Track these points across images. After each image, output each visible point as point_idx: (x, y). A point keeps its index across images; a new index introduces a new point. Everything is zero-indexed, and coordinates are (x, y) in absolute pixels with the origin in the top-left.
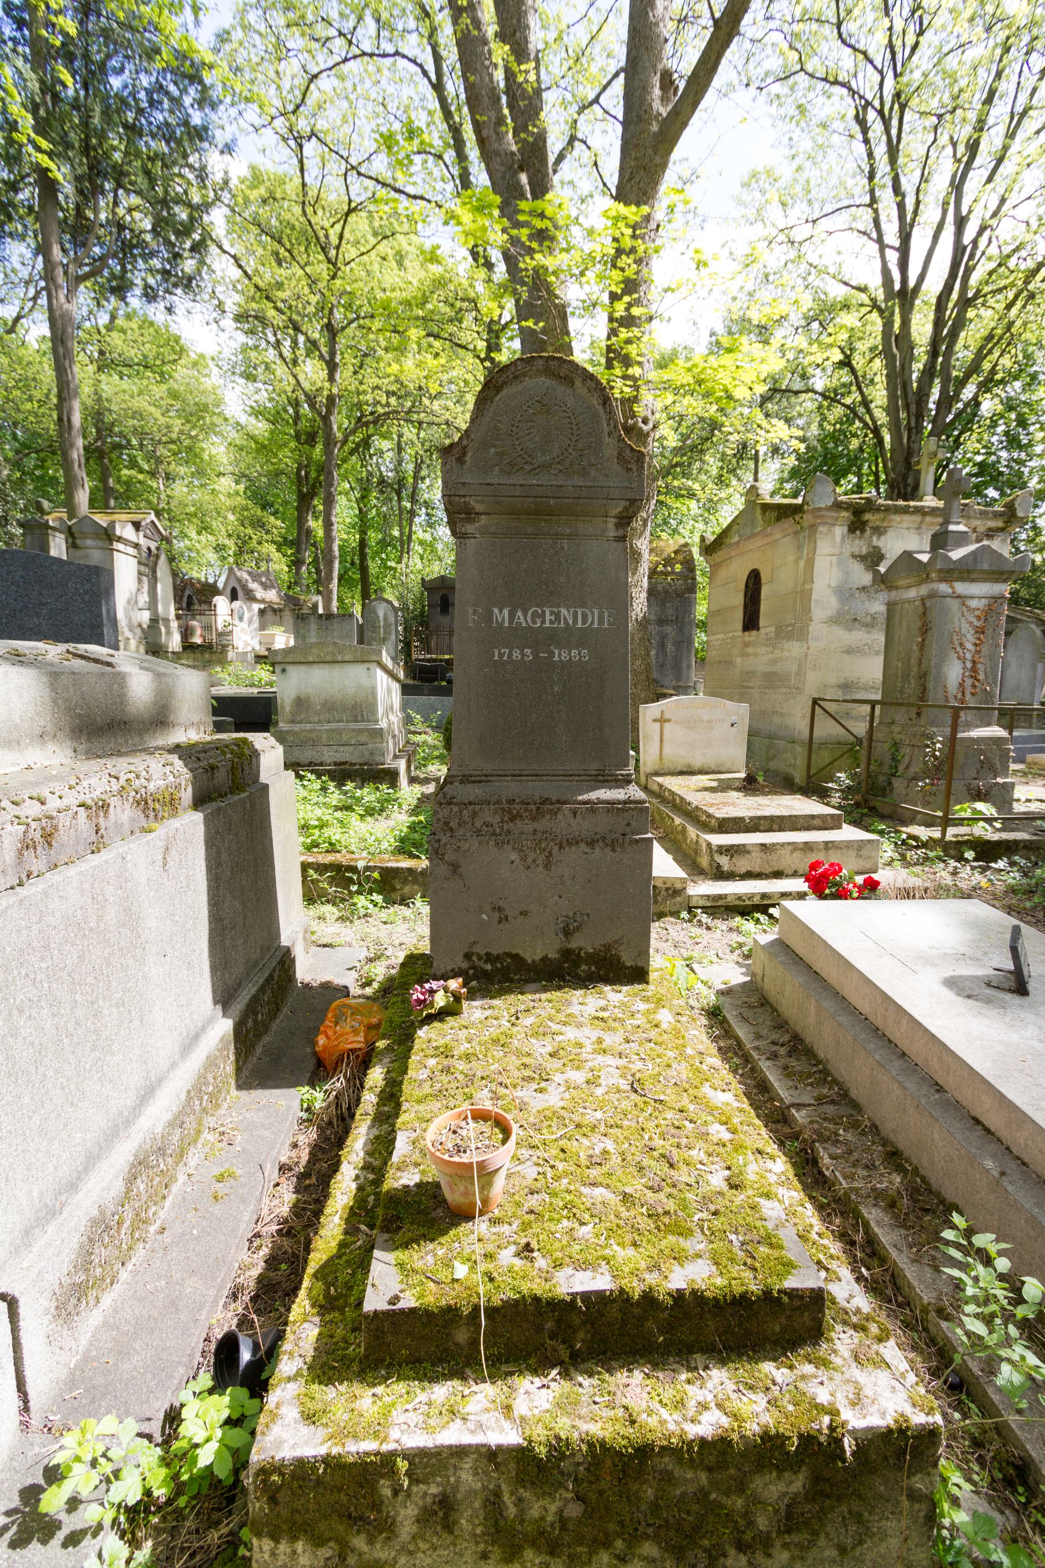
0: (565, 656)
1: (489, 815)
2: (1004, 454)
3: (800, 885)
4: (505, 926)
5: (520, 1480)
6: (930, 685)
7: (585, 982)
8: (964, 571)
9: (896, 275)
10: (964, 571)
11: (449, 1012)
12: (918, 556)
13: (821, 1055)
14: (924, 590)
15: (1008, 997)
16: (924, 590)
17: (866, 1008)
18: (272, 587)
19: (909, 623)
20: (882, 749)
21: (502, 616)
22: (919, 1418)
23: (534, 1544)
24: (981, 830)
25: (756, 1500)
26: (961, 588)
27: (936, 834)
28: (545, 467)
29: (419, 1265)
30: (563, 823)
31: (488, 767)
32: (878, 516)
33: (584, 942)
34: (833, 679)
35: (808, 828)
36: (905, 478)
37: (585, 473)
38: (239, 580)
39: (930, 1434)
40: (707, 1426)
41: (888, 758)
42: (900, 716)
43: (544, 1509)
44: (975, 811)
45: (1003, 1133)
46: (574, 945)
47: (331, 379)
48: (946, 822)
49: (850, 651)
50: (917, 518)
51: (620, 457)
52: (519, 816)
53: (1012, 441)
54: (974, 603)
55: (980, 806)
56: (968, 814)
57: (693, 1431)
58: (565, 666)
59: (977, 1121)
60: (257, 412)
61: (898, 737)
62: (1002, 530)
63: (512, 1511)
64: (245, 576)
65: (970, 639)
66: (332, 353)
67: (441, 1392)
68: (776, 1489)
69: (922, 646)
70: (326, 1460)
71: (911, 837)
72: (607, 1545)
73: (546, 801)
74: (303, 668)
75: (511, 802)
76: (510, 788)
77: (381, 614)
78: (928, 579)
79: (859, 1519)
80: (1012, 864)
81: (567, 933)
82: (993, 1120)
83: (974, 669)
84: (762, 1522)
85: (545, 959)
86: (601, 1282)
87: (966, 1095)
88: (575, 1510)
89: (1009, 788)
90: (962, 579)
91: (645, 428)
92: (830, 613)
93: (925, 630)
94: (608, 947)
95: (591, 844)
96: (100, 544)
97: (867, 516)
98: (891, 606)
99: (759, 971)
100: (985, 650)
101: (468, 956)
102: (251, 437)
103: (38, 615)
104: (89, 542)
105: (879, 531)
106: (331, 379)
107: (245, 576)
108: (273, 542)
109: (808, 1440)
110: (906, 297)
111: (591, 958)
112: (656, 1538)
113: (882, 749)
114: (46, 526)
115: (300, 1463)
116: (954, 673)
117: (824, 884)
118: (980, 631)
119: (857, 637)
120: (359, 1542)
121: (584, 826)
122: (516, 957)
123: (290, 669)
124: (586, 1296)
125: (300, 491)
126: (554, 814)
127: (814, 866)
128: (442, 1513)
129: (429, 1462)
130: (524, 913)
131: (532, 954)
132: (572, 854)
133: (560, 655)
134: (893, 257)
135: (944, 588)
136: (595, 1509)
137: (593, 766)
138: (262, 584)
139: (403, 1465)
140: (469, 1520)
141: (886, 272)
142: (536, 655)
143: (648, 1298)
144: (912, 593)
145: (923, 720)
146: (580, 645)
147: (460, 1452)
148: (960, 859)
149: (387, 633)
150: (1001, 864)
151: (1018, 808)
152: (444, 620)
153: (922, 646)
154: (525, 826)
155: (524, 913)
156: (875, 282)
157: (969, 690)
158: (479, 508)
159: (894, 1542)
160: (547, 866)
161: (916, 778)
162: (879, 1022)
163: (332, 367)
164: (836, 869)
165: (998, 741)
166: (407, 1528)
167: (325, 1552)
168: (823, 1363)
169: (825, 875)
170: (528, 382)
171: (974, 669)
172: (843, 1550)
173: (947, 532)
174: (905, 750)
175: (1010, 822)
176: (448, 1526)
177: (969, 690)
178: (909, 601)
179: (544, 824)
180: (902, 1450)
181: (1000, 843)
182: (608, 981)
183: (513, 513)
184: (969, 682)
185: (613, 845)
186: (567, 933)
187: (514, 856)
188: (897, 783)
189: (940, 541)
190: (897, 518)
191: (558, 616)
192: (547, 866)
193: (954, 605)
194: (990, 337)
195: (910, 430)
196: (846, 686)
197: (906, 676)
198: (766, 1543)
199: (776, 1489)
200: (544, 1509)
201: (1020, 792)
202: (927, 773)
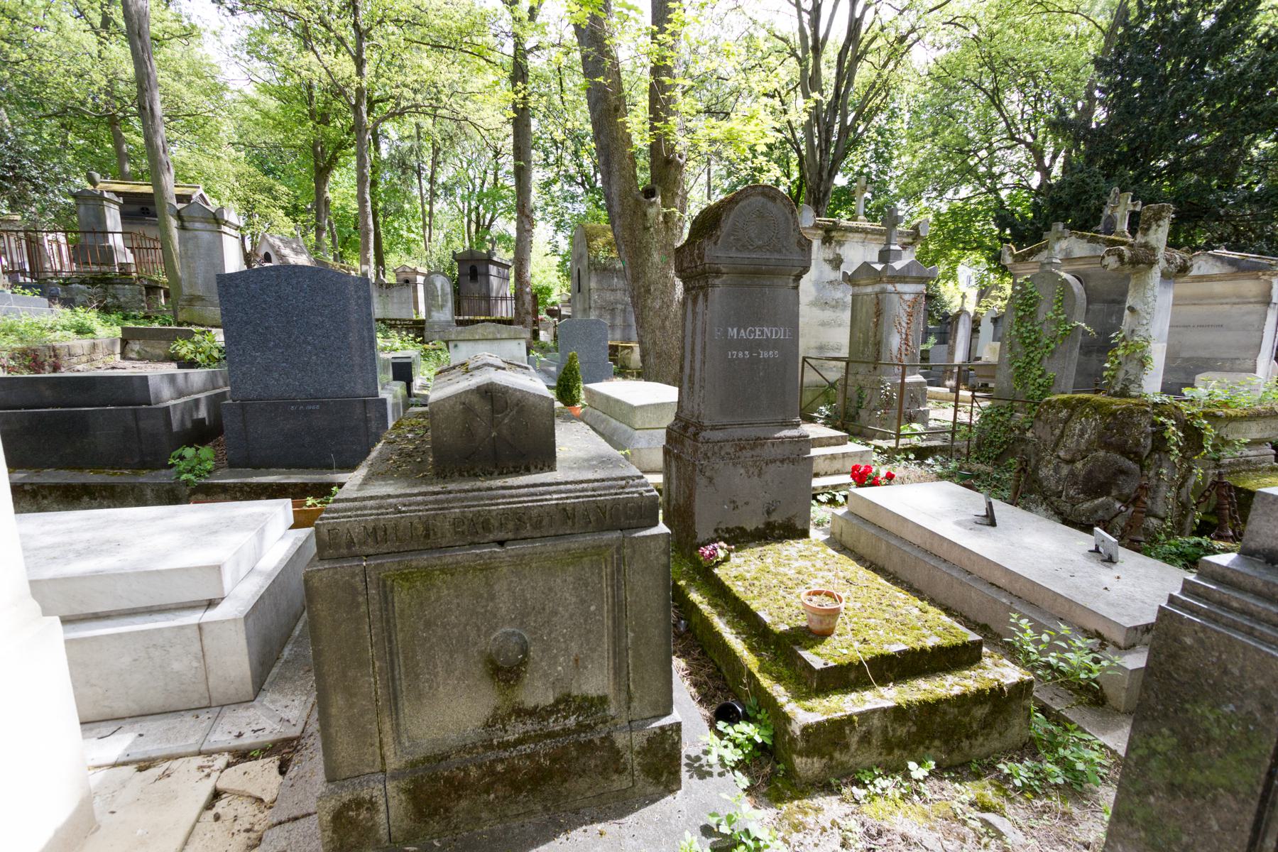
0: (766, 355)
1: (728, 448)
2: (873, 166)
3: (847, 479)
4: (737, 512)
5: (895, 720)
6: (883, 350)
7: (780, 539)
8: (901, 277)
9: (809, 32)
10: (901, 277)
11: (726, 559)
12: (875, 266)
13: (891, 570)
14: (877, 288)
15: (988, 528)
16: (877, 288)
17: (918, 541)
18: (303, 252)
19: (867, 309)
20: (852, 390)
21: (733, 332)
22: (1027, 678)
23: (898, 747)
24: (915, 441)
25: (973, 718)
26: (900, 287)
27: (892, 443)
28: (760, 247)
29: (824, 651)
30: (768, 452)
31: (725, 421)
32: (840, 233)
33: (777, 518)
34: (813, 343)
35: (829, 445)
36: (819, 186)
37: (780, 251)
38: (272, 246)
39: (1031, 683)
40: (957, 690)
41: (855, 397)
42: (862, 369)
43: (902, 731)
44: (912, 429)
45: (1008, 587)
46: (772, 519)
47: (360, 73)
48: (899, 436)
49: (823, 324)
50: (863, 235)
51: (799, 242)
52: (744, 448)
53: (878, 156)
54: (906, 297)
55: (915, 426)
56: (909, 432)
57: (953, 693)
58: (766, 360)
59: (992, 584)
60: (266, 89)
61: (862, 383)
62: (911, 244)
63: (891, 734)
64: (278, 242)
65: (904, 319)
66: (360, 51)
67: (854, 696)
68: (980, 712)
69: (877, 324)
70: (827, 720)
71: (876, 447)
72: (921, 743)
73: (759, 438)
74: (470, 344)
75: (740, 440)
76: (738, 433)
77: (439, 285)
78: (881, 281)
79: (1007, 721)
80: (936, 460)
81: (769, 513)
82: (1002, 582)
83: (906, 339)
84: (975, 726)
85: (757, 529)
86: (903, 647)
87: (985, 573)
88: (914, 729)
89: (926, 413)
90: (900, 282)
91: (682, 161)
92: (811, 298)
93: (879, 313)
94: (789, 519)
95: (782, 461)
96: (209, 227)
97: (834, 234)
98: (855, 297)
99: (837, 530)
100: (912, 326)
101: (716, 531)
102: (266, 115)
103: (322, 315)
104: (198, 225)
105: (840, 243)
106: (360, 73)
107: (278, 242)
108: (283, 208)
109: (992, 690)
110: (818, 48)
111: (782, 526)
112: (939, 738)
113: (852, 390)
114: (101, 197)
115: (818, 723)
116: (895, 341)
117: (862, 477)
118: (910, 315)
119: (828, 314)
120: (837, 755)
121: (778, 452)
122: (742, 529)
123: (461, 345)
124: (899, 652)
125: (316, 165)
126: (762, 445)
127: (855, 468)
128: (865, 739)
129: (865, 716)
130: (747, 503)
131: (750, 526)
132: (772, 467)
133: (764, 354)
134: (806, 17)
135: (890, 287)
136: (922, 727)
137: (780, 418)
138: (293, 249)
139: (856, 718)
140: (875, 741)
141: (802, 30)
142: (751, 354)
143: (923, 650)
144: (869, 289)
145: (878, 372)
146: (774, 348)
147: (874, 711)
148: (907, 459)
149: (444, 301)
150: (930, 461)
151: (932, 424)
152: (474, 287)
153: (877, 324)
154: (747, 453)
155: (747, 503)
156: (795, 40)
157: (904, 352)
158: (724, 270)
159: (1017, 728)
160: (759, 476)
161: (875, 409)
162: (928, 547)
163: (360, 62)
164: (868, 468)
165: (920, 384)
166: (854, 747)
167: (824, 761)
168: (984, 668)
169: (865, 473)
170: (752, 199)
171: (906, 339)
172: (1000, 734)
173: (889, 250)
174: (867, 392)
175: (934, 433)
176: (869, 743)
177: (904, 352)
178: (867, 294)
179: (758, 451)
180: (1022, 689)
181: (927, 448)
182: (793, 538)
183: (742, 273)
184: (904, 347)
185: (793, 462)
186: (769, 513)
187: (742, 471)
188: (862, 413)
189: (885, 256)
190: (851, 235)
191: (762, 332)
192: (759, 476)
193: (895, 298)
194: (873, 86)
195: (821, 151)
196: (821, 348)
197: (866, 343)
198: (976, 734)
199: (980, 712)
200: (902, 731)
201: (932, 414)
202: (882, 406)
